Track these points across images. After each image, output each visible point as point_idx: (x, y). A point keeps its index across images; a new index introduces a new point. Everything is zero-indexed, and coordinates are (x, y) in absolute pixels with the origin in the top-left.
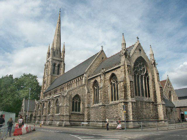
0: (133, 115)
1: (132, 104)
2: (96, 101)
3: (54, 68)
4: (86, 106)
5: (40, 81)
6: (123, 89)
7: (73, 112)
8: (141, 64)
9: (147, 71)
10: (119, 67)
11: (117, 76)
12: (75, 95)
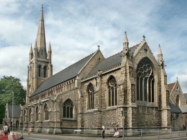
0: (132, 121)
1: (133, 109)
2: (91, 106)
4: (79, 111)
5: (24, 85)
7: (64, 118)
8: (146, 65)
9: (152, 73)
10: (120, 69)
11: (117, 79)
12: (66, 99)
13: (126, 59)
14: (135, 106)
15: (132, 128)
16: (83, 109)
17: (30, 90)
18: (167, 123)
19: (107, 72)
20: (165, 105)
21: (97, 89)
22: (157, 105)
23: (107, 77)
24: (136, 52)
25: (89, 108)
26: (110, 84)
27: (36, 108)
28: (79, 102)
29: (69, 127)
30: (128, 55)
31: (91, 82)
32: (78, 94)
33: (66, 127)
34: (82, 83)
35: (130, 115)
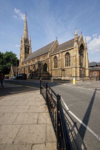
2: (56, 67)
3: (26, 50)
4: (50, 69)
5: (18, 58)
6: (75, 61)
7: (44, 72)
10: (73, 48)
11: (71, 54)
12: (45, 63)
15: (80, 77)
17: (22, 60)
18: (88, 75)
19: (65, 50)
22: (84, 67)
23: (65, 53)
25: (55, 67)
26: (66, 56)
27: (24, 68)
28: (50, 65)
31: (56, 55)
32: (49, 61)
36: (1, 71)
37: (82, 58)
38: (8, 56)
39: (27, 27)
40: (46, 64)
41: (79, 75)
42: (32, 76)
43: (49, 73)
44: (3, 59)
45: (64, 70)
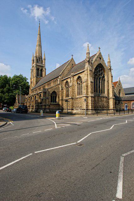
0: (91, 105)
1: (91, 98)
2: (67, 96)
3: (38, 72)
4: (60, 99)
7: (51, 103)
8: (100, 69)
10: (84, 71)
12: (53, 91)
13: (88, 65)
14: (93, 96)
15: (91, 110)
16: (62, 97)
17: (32, 85)
18: (112, 107)
20: (112, 95)
21: (70, 84)
22: (106, 96)
23: (77, 77)
24: (94, 60)
26: (78, 81)
27: (34, 97)
28: (60, 93)
29: (54, 108)
30: (89, 61)
33: (53, 108)
34: (62, 81)
35: (90, 102)
36: (7, 101)
37: (101, 83)
38: (16, 82)
39: (40, 41)
40: (54, 92)
41: (90, 107)
42: (38, 109)
43: (59, 105)
44: (9, 85)
45: (67, 100)
